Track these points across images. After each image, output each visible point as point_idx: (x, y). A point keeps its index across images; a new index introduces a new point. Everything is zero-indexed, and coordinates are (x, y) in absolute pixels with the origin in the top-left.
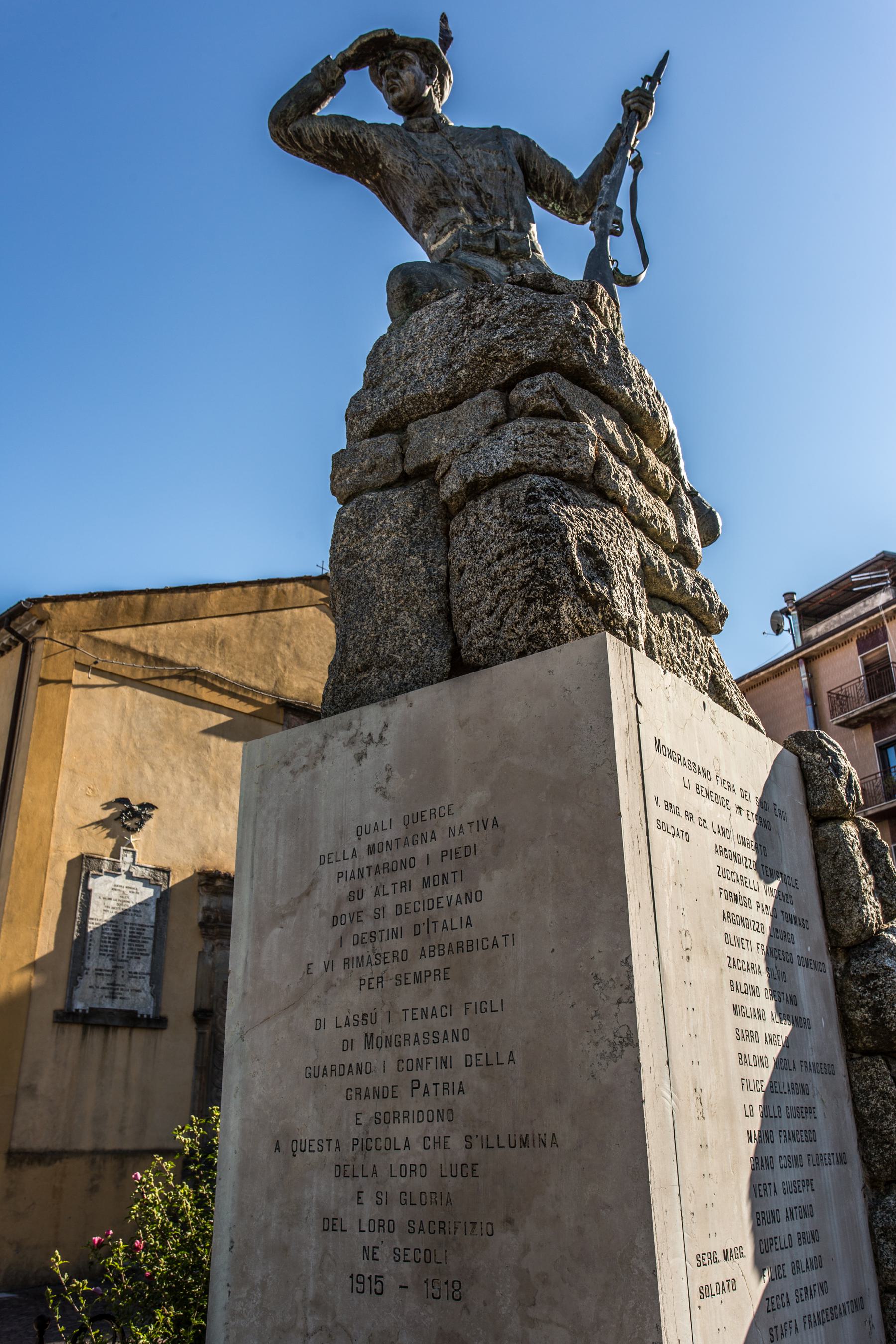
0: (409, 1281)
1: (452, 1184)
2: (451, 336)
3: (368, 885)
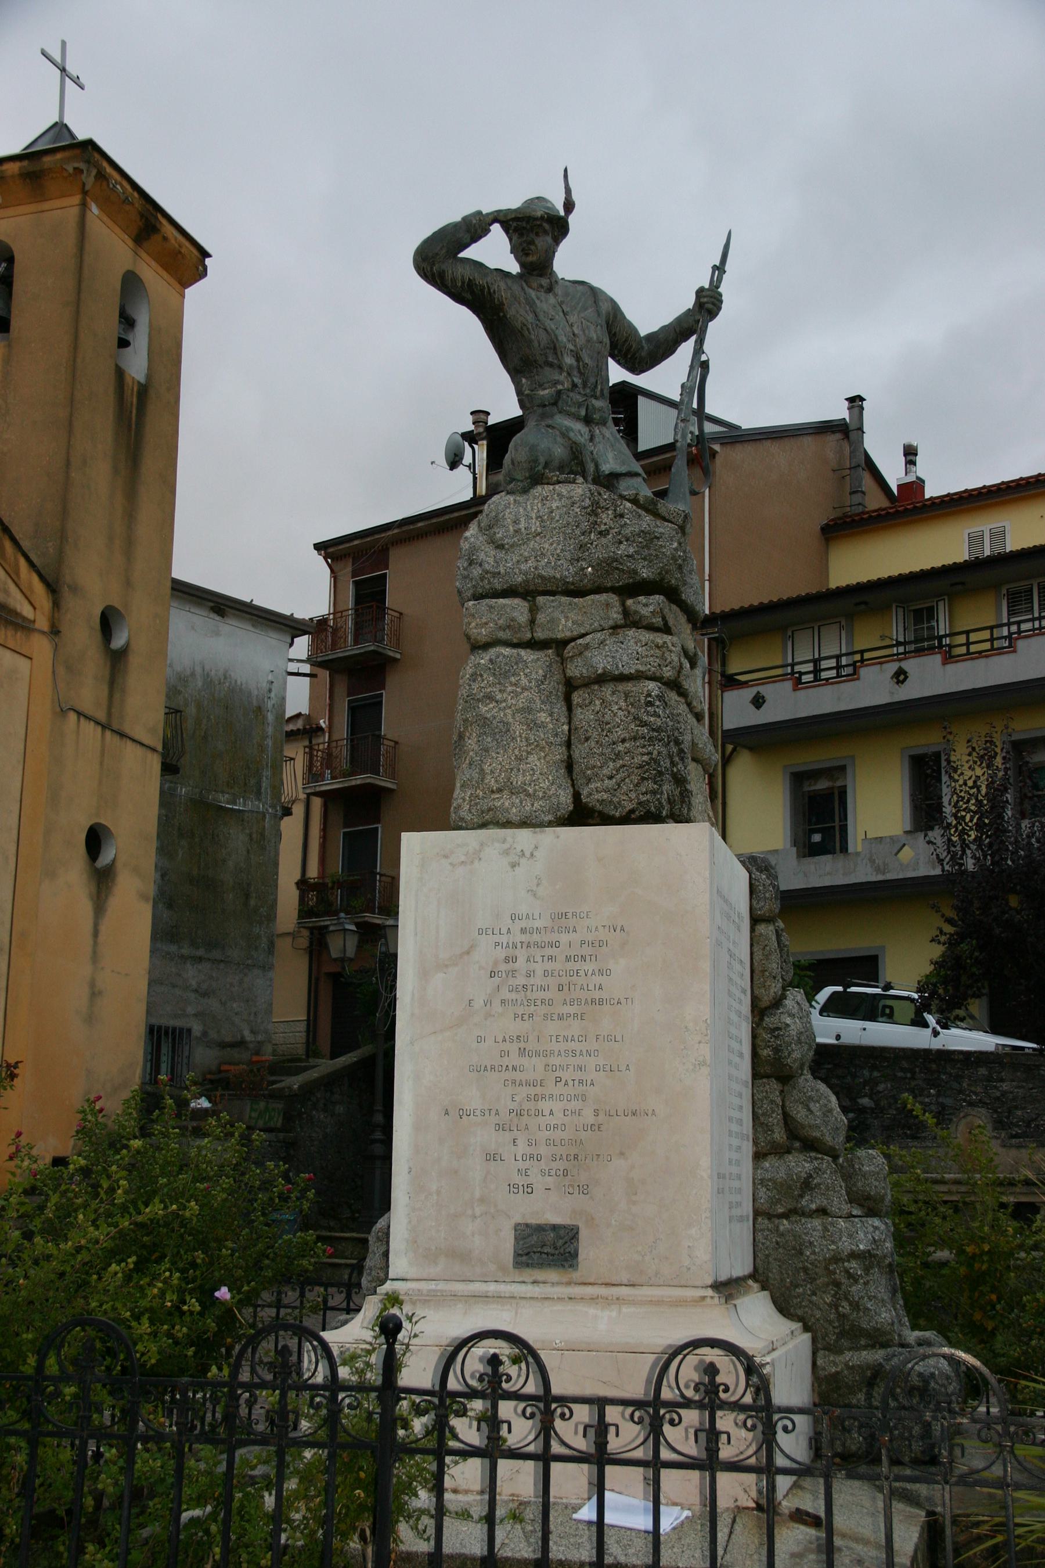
0: (551, 1187)
1: (583, 1135)
2: (578, 532)
3: (522, 955)
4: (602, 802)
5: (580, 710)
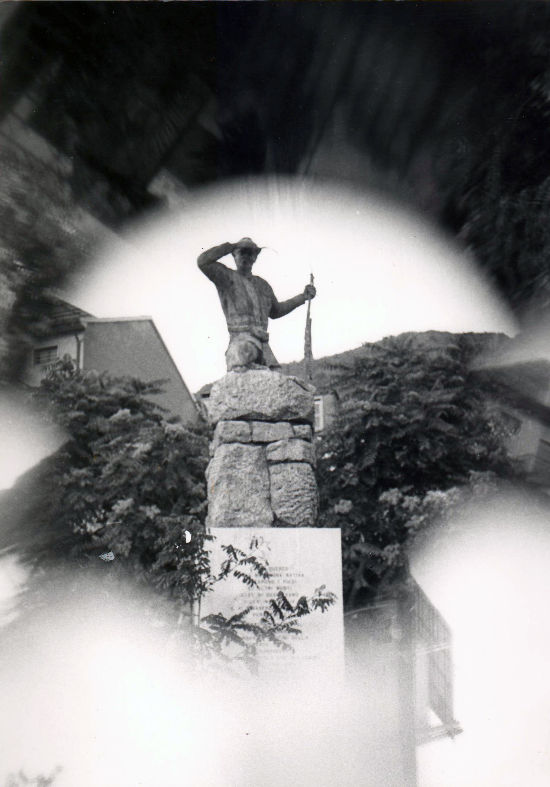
4: (287, 518)
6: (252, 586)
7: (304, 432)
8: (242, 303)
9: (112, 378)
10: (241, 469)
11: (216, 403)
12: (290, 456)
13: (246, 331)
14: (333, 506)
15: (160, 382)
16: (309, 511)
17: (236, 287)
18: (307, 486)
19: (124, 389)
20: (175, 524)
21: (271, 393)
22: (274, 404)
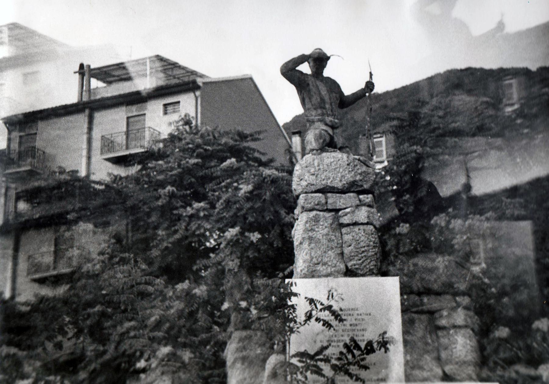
4: (357, 269)
5: (346, 235)
6: (330, 329)
7: (368, 200)
8: (316, 99)
9: (222, 131)
10: (318, 231)
11: (298, 180)
12: (357, 220)
13: (320, 120)
14: (395, 229)
15: (259, 133)
16: (373, 263)
17: (311, 87)
18: (372, 243)
19: (232, 138)
20: (267, 286)
21: (341, 170)
22: (343, 180)
